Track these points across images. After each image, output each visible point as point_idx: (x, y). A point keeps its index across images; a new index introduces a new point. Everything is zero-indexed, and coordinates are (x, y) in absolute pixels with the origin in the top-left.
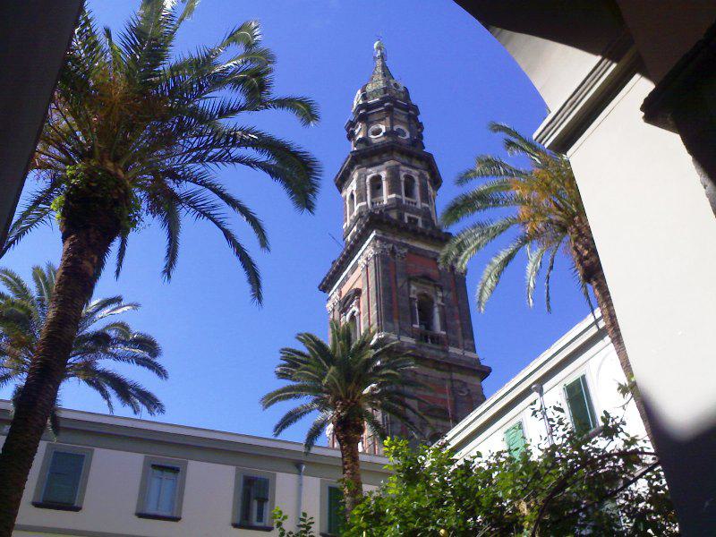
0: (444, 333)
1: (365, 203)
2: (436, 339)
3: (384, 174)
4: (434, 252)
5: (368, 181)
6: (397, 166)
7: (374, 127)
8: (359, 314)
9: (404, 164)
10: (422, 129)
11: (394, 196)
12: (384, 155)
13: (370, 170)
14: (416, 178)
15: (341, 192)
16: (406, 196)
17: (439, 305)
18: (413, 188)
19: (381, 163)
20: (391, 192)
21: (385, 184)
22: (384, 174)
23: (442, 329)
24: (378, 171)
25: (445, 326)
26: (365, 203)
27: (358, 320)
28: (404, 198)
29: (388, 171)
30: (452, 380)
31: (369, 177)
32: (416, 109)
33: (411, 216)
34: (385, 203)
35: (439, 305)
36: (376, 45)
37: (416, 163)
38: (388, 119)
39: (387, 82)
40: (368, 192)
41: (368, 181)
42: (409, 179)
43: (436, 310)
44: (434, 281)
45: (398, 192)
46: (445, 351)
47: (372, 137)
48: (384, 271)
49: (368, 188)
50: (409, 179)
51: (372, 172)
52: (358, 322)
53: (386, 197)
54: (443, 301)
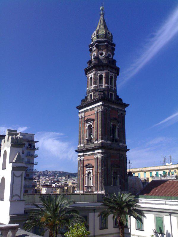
0: (118, 138)
1: (96, 85)
2: (116, 141)
3: (104, 75)
4: (118, 108)
5: (98, 76)
6: (108, 73)
7: (100, 52)
8: (93, 128)
9: (111, 72)
10: (118, 73)
11: (107, 85)
12: (104, 67)
13: (99, 72)
14: (113, 77)
15: (86, 75)
16: (110, 85)
17: (118, 128)
18: (115, 132)
19: (103, 70)
20: (106, 83)
21: (104, 79)
22: (104, 75)
23: (118, 137)
24: (102, 73)
25: (119, 136)
26: (96, 85)
27: (92, 129)
28: (110, 86)
29: (106, 74)
30: (119, 154)
31: (99, 75)
32: (114, 45)
33: (111, 93)
34: (104, 87)
35: (118, 128)
36: (101, 8)
37: (114, 71)
38: (106, 50)
39: (106, 32)
40: (98, 81)
41: (98, 76)
42: (111, 77)
43: (117, 130)
44: (117, 120)
45: (108, 84)
46: (118, 144)
47: (100, 56)
48: (104, 117)
49: (98, 79)
50: (111, 77)
51: (100, 73)
52: (92, 130)
53: (104, 85)
54: (119, 127)
